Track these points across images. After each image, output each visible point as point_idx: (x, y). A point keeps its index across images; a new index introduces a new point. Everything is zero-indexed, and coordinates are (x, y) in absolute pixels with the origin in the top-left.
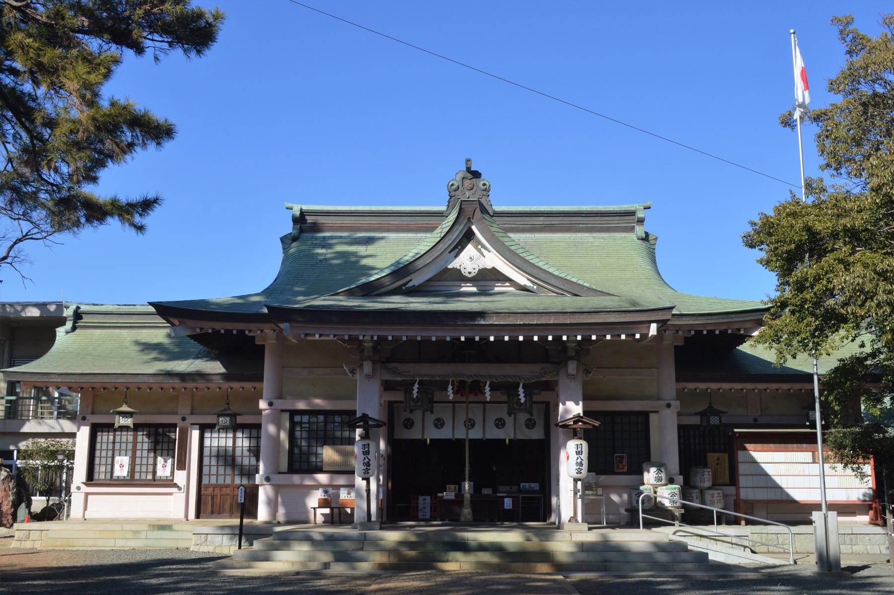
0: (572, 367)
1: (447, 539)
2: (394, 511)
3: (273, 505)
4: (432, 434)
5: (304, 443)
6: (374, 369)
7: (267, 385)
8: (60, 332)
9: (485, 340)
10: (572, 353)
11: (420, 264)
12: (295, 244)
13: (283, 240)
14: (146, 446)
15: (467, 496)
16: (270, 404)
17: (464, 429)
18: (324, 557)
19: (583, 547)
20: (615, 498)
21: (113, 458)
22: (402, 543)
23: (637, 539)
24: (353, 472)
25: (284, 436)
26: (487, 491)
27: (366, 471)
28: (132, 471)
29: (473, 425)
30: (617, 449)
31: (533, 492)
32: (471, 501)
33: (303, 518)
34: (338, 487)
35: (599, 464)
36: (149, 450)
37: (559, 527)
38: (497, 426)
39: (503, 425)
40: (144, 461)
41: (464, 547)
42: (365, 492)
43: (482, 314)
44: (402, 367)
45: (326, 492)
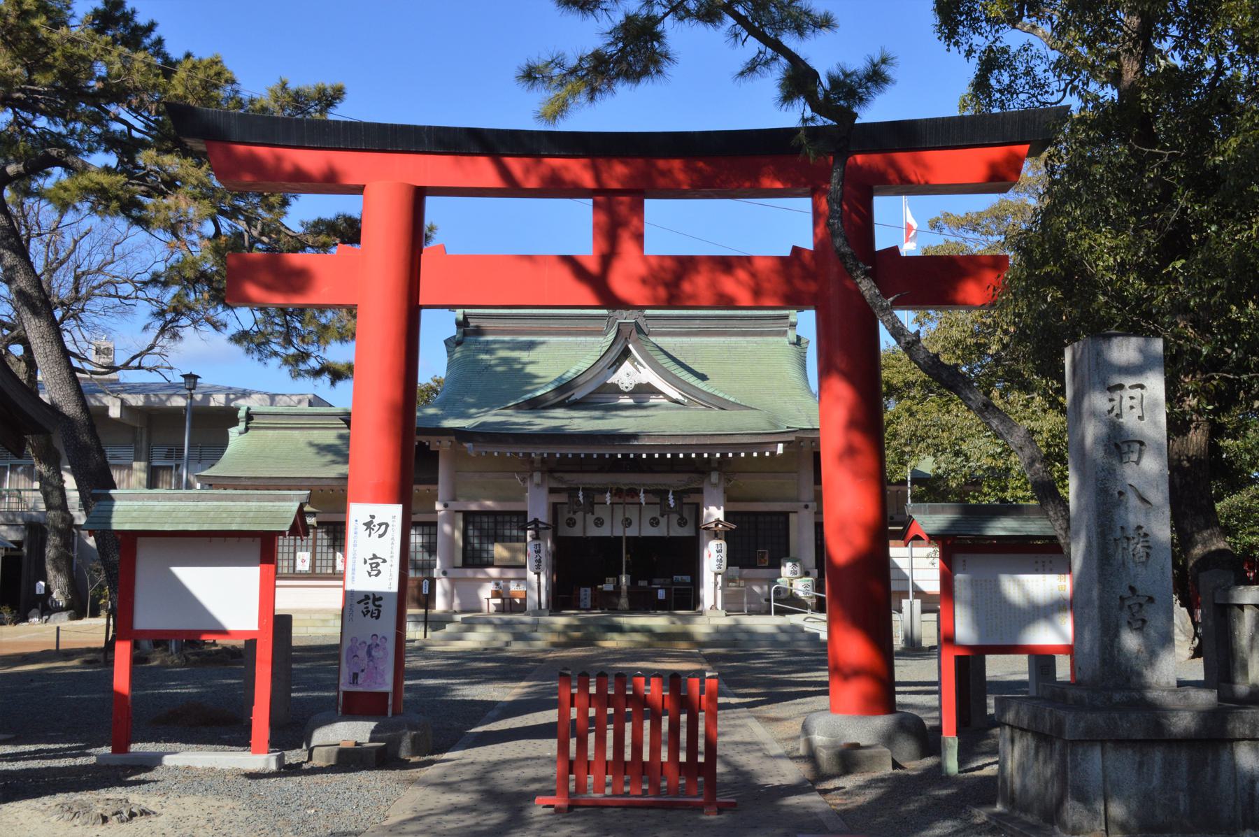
0: (714, 477)
1: (605, 623)
2: (560, 599)
3: (449, 596)
4: (594, 532)
5: (476, 541)
6: (543, 481)
7: (442, 488)
8: (233, 432)
9: (638, 456)
10: (715, 465)
11: (581, 380)
12: (458, 349)
13: (447, 342)
14: (325, 543)
15: (624, 588)
16: (446, 506)
17: (621, 527)
18: (504, 637)
19: (718, 630)
20: (757, 589)
21: (295, 553)
22: (568, 627)
23: (765, 624)
24: (525, 567)
25: (458, 535)
26: (642, 583)
27: (538, 567)
28: (313, 566)
29: (630, 524)
30: (757, 544)
31: (685, 583)
32: (628, 592)
33: (476, 607)
34: (509, 580)
35: (738, 557)
36: (328, 546)
37: (701, 613)
38: (652, 524)
39: (658, 523)
40: (324, 556)
41: (619, 629)
42: (535, 584)
43: (635, 436)
44: (567, 477)
45: (497, 584)
